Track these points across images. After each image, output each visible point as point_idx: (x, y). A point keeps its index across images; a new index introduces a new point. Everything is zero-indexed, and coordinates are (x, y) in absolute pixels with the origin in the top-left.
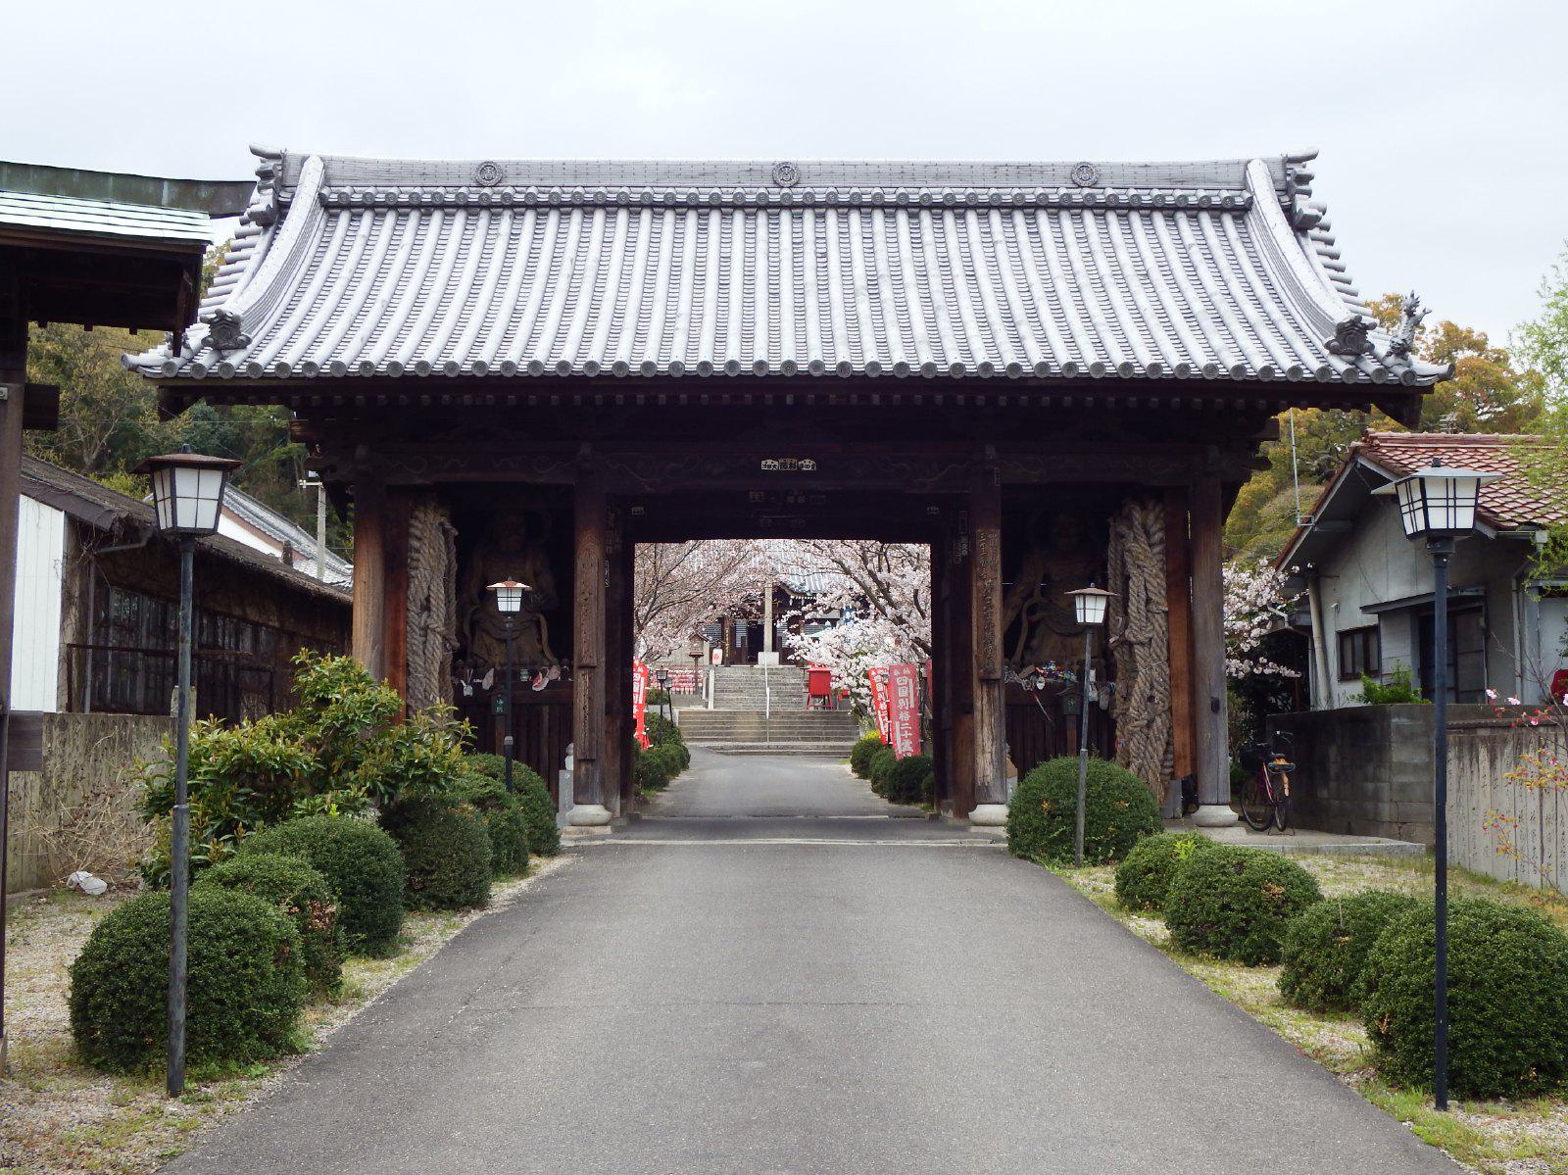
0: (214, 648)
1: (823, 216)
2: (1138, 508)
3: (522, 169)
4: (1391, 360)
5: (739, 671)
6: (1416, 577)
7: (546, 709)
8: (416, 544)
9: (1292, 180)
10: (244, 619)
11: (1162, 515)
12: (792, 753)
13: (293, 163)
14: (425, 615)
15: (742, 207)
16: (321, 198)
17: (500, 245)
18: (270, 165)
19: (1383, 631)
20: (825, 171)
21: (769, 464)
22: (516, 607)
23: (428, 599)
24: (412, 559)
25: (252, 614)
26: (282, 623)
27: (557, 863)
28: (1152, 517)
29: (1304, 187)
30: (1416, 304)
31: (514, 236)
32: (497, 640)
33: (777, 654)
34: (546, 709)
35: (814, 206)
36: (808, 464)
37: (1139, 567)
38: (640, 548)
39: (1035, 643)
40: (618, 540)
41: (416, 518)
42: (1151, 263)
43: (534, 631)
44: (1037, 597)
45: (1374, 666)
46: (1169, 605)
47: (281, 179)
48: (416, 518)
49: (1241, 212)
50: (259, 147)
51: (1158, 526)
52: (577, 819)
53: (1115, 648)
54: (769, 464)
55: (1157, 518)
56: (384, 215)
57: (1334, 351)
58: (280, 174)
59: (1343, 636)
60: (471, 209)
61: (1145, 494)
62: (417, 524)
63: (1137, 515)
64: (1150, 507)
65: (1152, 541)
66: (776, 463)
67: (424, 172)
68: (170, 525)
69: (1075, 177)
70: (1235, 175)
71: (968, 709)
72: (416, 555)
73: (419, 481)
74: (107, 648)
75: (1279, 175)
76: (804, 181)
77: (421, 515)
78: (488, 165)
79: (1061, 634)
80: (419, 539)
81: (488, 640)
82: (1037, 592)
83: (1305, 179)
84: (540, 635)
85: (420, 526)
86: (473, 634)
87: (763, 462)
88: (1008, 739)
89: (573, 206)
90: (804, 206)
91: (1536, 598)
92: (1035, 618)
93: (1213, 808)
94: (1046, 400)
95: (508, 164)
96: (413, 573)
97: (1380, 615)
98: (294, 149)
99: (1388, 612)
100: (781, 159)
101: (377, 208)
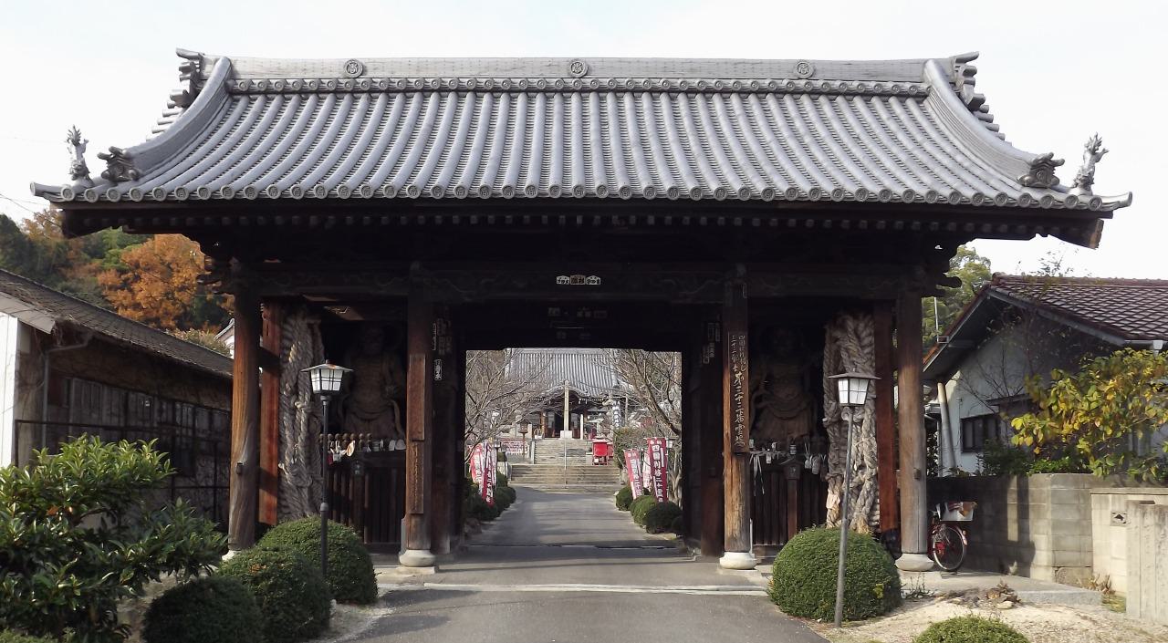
0: (173, 425)
2: (851, 318)
3: (382, 64)
9: (962, 71)
10: (199, 405)
11: (871, 323)
16: (226, 85)
17: (355, 117)
21: (563, 279)
25: (206, 402)
27: (379, 613)
28: (862, 325)
29: (969, 79)
32: (362, 419)
33: (571, 432)
36: (594, 280)
37: (853, 362)
38: (474, 358)
39: (760, 424)
40: (448, 344)
42: (858, 130)
44: (762, 391)
46: (877, 394)
49: (921, 97)
50: (181, 53)
51: (868, 331)
53: (828, 426)
54: (563, 279)
55: (866, 326)
57: (1029, 185)
58: (198, 70)
61: (861, 307)
63: (850, 324)
64: (861, 318)
65: (863, 344)
66: (568, 279)
68: (319, 389)
71: (719, 476)
73: (285, 293)
74: (42, 423)
77: (293, 322)
78: (353, 62)
79: (781, 418)
82: (762, 387)
84: (394, 415)
85: (290, 329)
86: (345, 413)
87: (558, 278)
92: (761, 405)
94: (792, 222)
96: (285, 366)
98: (209, 54)
100: (573, 55)
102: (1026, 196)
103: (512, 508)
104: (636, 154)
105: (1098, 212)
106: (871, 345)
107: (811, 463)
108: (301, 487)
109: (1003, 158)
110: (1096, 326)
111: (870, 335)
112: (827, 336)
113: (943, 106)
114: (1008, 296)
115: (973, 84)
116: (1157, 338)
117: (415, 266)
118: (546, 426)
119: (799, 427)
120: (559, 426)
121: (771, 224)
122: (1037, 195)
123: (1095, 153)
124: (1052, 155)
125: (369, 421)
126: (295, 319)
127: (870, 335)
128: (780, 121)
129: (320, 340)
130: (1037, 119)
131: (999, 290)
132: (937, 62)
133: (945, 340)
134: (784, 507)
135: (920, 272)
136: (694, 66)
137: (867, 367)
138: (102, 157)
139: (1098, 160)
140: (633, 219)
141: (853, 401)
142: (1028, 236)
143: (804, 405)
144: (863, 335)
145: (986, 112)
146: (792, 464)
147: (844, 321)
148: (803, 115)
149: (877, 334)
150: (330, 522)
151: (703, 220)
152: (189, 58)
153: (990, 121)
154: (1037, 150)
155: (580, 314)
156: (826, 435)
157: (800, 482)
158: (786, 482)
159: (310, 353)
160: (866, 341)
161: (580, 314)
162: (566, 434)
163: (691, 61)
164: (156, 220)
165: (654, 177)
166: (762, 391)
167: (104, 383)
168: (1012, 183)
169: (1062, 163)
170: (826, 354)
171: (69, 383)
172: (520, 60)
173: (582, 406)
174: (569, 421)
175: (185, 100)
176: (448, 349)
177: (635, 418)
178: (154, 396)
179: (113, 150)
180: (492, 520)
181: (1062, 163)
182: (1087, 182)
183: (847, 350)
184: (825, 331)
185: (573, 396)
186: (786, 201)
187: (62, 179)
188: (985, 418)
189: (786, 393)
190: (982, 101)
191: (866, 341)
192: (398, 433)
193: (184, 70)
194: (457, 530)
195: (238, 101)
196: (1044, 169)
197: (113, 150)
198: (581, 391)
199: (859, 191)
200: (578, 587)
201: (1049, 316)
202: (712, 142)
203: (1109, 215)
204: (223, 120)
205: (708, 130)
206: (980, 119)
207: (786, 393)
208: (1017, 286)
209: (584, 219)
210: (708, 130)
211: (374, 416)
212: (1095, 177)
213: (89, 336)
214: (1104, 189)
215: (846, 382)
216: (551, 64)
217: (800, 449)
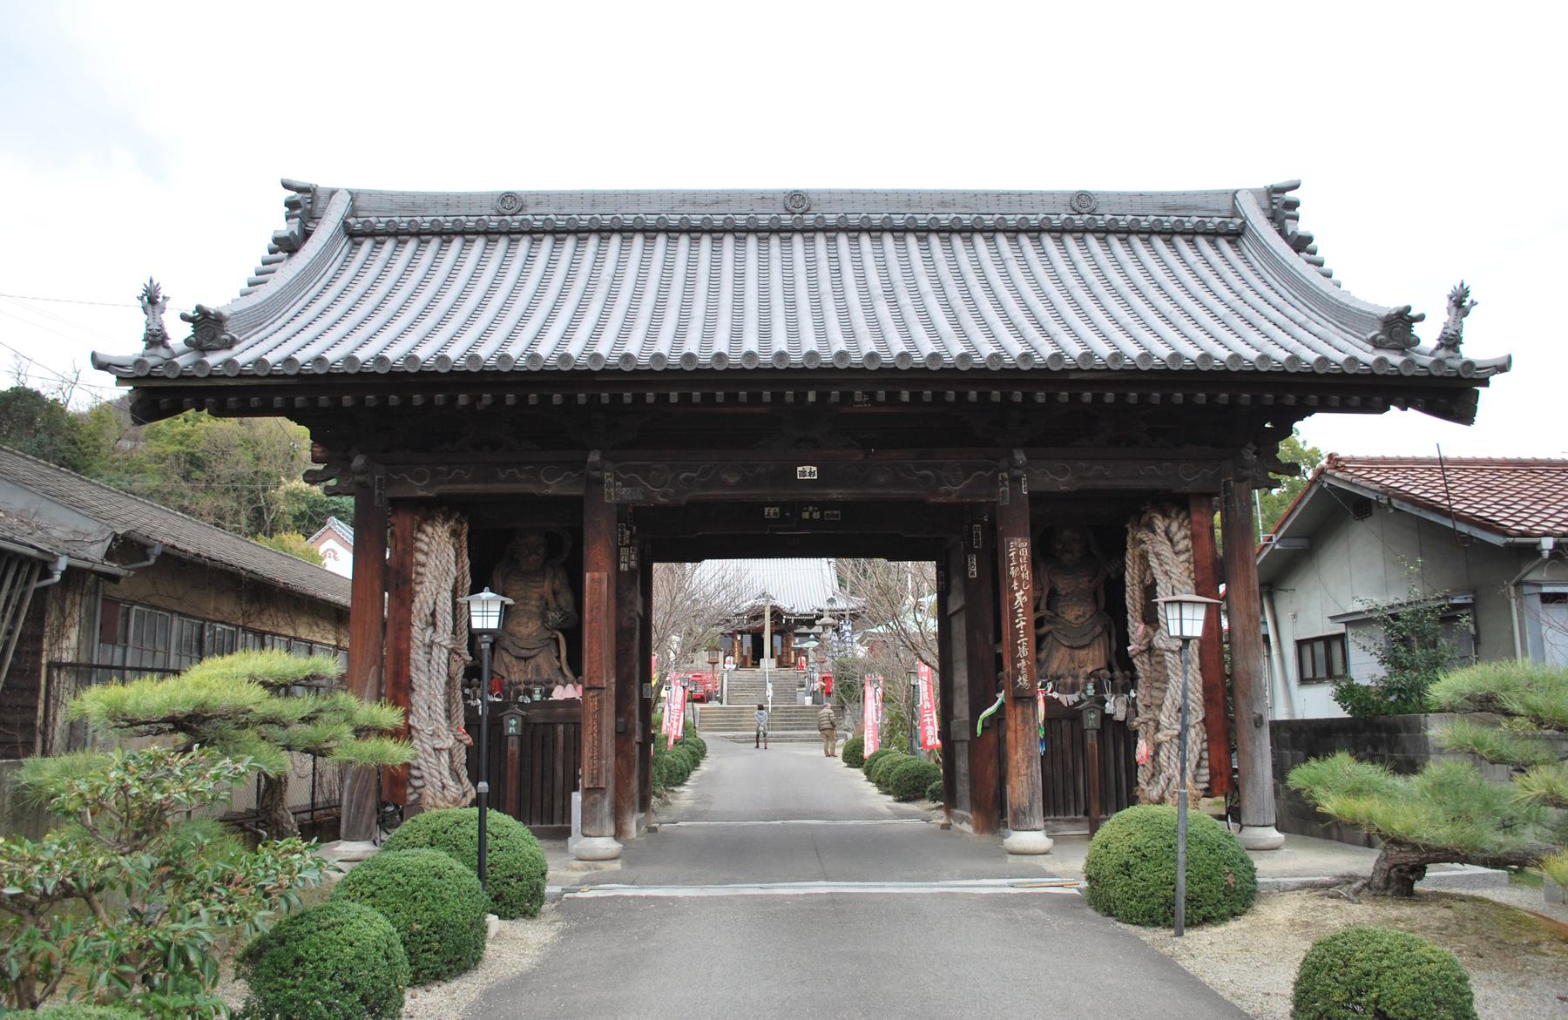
1: (835, 239)
4: (1442, 353)
5: (746, 674)
6: (1386, 587)
7: (561, 728)
8: (421, 557)
9: (1280, 205)
12: (791, 740)
13: (323, 197)
14: (430, 631)
15: (755, 231)
16: (345, 224)
18: (298, 196)
19: (1350, 637)
20: (834, 197)
22: (493, 623)
23: (433, 614)
24: (418, 574)
26: (338, 641)
30: (1466, 293)
31: (530, 259)
34: (561, 728)
35: (825, 230)
38: (658, 567)
41: (424, 532)
43: (554, 650)
44: (1044, 611)
45: (1338, 670)
47: (310, 211)
48: (424, 532)
51: (1183, 533)
52: (587, 855)
56: (405, 242)
59: (1300, 644)
60: (490, 234)
61: (1177, 503)
62: (424, 537)
63: (1160, 524)
67: (448, 201)
69: (1076, 205)
70: (1225, 205)
72: (421, 570)
75: (1266, 204)
76: (814, 209)
77: (429, 529)
78: (509, 195)
79: (1071, 647)
80: (426, 554)
81: (507, 658)
83: (1294, 205)
88: (1018, 746)
89: (590, 231)
90: (815, 230)
91: (1537, 600)
92: (1044, 630)
93: (1259, 830)
95: (529, 194)
96: (418, 588)
97: (1346, 623)
98: (322, 181)
99: (1357, 621)
100: (1268, 184)
101: (399, 235)
102: (1382, 361)
103: (705, 766)
104: (883, 309)
105: (1471, 379)
106: (1187, 550)
107: (1115, 706)
108: (440, 750)
109: (1344, 315)
110: (1469, 520)
111: (1185, 537)
112: (1129, 539)
113: (1263, 248)
114: (1350, 483)
115: (1296, 218)
116: (1546, 535)
117: (594, 457)
118: (741, 653)
119: (1094, 658)
120: (757, 653)
121: (1060, 400)
122: (1395, 359)
123: (1460, 303)
124: (1408, 309)
125: (526, 659)
126: (433, 526)
127: (1185, 537)
128: (1062, 267)
129: (465, 552)
130: (1379, 260)
131: (1338, 475)
132: (1254, 192)
133: (1270, 539)
134: (1093, 772)
135: (1250, 456)
136: (948, 198)
137: (1184, 579)
138: (184, 318)
139: (1466, 314)
140: (881, 395)
141: (1187, 633)
142: (1383, 409)
143: (1098, 629)
144: (1176, 538)
145: (1314, 253)
146: (1090, 709)
147: (1151, 519)
148: (1091, 258)
149: (1194, 537)
150: (494, 815)
151: (973, 395)
152: (299, 190)
153: (1320, 264)
154: (1389, 303)
155: (806, 515)
156: (1132, 668)
157: (1101, 733)
158: (1083, 732)
159: (453, 568)
160: (1181, 546)
161: (806, 515)
162: (768, 664)
163: (909, 193)
164: (255, 401)
165: (910, 340)
166: (1044, 611)
167: (172, 612)
168: (1361, 344)
169: (1421, 318)
170: (1129, 563)
171: (127, 614)
172: (723, 192)
173: (787, 625)
174: (787, 657)
175: (287, 246)
176: (633, 564)
177: (860, 641)
178: (237, 627)
179: (199, 309)
180: (680, 784)
181: (1421, 318)
182: (1451, 341)
183: (1157, 555)
184: (1126, 532)
185: (777, 613)
186: (1079, 370)
187: (129, 345)
188: (1328, 640)
189: (1074, 613)
190: (1310, 239)
191: (1181, 546)
192: (565, 676)
193: (291, 205)
194: (644, 805)
195: (360, 244)
196: (1398, 326)
197: (199, 309)
198: (784, 604)
199: (1172, 356)
200: (821, 888)
201: (1407, 508)
202: (978, 292)
203: (1485, 382)
204: (341, 270)
205: (972, 278)
206: (1309, 262)
207: (1074, 613)
208: (1360, 469)
209: (818, 396)
210: (972, 278)
211: (533, 653)
212: (1464, 335)
213: (157, 550)
214: (1475, 349)
215: (1177, 607)
216: (763, 197)
217: (1099, 688)
